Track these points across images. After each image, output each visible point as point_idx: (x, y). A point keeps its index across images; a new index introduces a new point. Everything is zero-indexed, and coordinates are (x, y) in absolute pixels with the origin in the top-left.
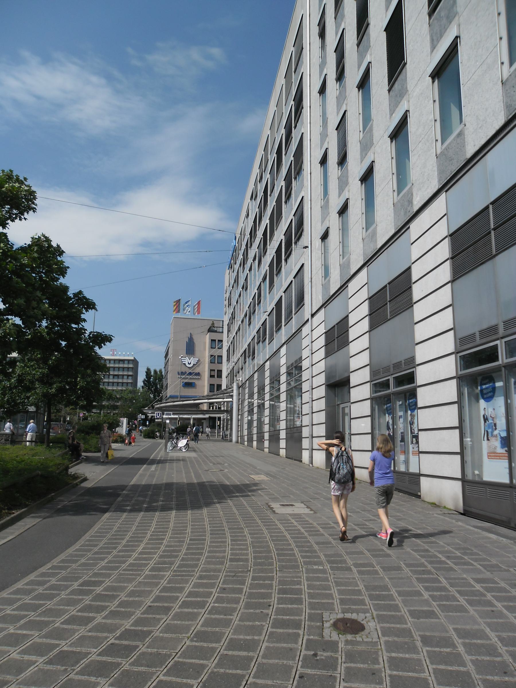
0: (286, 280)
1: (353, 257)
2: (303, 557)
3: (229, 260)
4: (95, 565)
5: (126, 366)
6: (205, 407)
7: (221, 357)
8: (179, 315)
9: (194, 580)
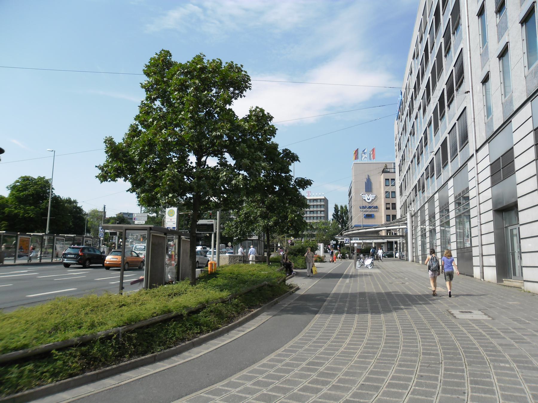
0: (449, 123)
1: (515, 95)
2: (488, 355)
3: (397, 112)
4: (316, 350)
5: (319, 203)
6: (383, 233)
7: (394, 192)
8: (358, 161)
9: (395, 367)
